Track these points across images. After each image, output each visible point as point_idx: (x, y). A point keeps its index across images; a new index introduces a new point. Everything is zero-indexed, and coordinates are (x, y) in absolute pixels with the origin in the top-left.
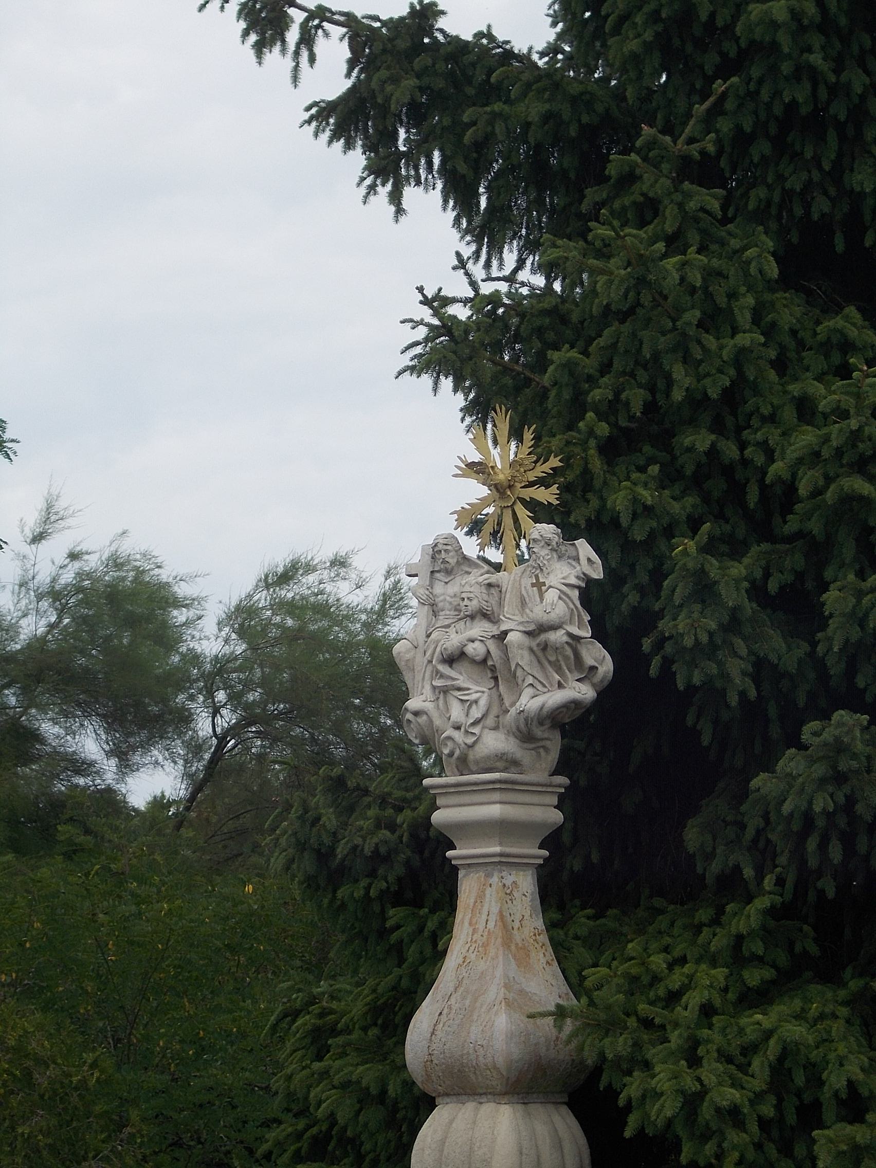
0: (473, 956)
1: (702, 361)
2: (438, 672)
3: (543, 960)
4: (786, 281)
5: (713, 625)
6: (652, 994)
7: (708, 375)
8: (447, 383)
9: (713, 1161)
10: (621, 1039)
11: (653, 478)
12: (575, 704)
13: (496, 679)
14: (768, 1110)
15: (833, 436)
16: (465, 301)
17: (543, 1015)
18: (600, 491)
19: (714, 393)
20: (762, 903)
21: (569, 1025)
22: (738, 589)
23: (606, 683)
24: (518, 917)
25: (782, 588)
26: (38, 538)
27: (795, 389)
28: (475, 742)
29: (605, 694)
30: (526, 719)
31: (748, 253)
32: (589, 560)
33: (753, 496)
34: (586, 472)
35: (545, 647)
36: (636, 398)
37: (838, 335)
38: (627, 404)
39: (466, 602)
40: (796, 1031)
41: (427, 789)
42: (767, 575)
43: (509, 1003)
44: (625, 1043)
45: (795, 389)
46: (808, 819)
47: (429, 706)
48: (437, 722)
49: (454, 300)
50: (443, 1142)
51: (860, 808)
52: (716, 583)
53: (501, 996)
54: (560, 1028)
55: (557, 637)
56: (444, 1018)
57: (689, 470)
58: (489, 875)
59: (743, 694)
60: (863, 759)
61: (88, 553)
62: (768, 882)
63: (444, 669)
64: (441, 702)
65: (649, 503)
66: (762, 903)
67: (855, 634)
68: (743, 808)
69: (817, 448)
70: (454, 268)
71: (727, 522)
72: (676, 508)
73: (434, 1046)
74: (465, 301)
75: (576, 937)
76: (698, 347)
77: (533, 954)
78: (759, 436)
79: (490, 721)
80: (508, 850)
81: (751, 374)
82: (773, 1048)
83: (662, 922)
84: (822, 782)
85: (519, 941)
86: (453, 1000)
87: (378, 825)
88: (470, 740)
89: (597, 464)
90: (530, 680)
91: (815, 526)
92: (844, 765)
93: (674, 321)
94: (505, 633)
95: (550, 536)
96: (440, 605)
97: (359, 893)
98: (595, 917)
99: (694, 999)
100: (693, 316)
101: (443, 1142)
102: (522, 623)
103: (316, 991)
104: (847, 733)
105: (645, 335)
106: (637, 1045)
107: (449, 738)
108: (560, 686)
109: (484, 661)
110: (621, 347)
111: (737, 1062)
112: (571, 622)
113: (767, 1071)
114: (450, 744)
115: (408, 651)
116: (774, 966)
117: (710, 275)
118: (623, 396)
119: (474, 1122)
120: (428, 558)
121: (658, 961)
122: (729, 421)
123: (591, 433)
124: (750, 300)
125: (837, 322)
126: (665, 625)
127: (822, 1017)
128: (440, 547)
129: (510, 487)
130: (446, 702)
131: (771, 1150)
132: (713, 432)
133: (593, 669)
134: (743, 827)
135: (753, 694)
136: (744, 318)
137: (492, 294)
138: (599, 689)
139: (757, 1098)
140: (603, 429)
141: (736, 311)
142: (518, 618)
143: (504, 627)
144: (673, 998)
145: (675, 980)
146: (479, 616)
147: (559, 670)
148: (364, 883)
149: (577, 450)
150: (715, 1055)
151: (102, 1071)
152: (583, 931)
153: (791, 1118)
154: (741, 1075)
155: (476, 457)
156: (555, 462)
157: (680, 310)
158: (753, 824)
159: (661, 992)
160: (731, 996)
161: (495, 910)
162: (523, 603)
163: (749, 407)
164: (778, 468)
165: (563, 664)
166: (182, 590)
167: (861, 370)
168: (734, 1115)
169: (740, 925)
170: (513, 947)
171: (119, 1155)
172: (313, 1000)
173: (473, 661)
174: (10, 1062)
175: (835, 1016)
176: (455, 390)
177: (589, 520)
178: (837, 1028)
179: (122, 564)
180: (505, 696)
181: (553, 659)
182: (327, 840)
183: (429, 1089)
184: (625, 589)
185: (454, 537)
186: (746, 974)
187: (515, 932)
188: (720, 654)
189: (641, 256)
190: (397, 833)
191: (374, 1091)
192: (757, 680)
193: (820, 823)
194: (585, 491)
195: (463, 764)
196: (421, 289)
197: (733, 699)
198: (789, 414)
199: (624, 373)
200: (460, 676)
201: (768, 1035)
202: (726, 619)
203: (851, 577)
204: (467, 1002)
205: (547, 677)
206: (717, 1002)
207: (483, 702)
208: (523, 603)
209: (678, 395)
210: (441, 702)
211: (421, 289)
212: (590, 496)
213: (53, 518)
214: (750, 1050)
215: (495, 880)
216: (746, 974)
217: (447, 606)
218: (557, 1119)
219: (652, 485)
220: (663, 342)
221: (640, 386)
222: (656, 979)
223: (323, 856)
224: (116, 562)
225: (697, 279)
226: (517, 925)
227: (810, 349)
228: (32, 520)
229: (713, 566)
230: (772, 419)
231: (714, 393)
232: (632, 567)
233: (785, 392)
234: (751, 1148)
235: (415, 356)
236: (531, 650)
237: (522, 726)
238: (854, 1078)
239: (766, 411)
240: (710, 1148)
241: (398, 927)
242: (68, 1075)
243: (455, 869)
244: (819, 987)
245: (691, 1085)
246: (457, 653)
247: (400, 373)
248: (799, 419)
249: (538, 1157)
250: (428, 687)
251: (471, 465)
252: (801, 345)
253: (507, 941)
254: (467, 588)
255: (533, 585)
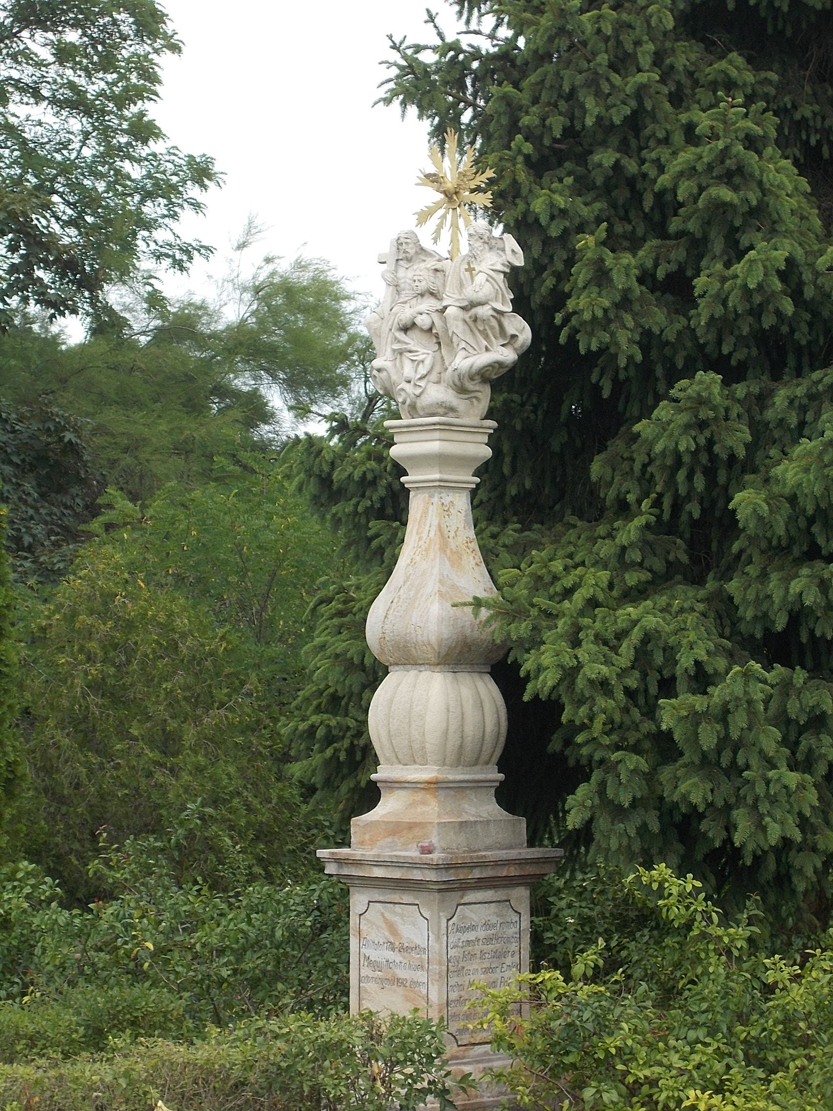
0: (418, 558)
1: (610, 94)
2: (396, 338)
3: (473, 562)
4: (676, 34)
5: (607, 303)
6: (552, 590)
7: (615, 105)
8: (413, 110)
9: (586, 721)
10: (524, 625)
11: (568, 187)
12: (500, 364)
13: (439, 344)
14: (632, 682)
15: (705, 154)
16: (435, 49)
17: (465, 604)
18: (526, 197)
19: (617, 120)
20: (639, 521)
21: (484, 613)
22: (627, 275)
23: (525, 348)
24: (454, 528)
25: (668, 276)
26: (241, 246)
27: (684, 118)
28: (421, 393)
29: (526, 357)
30: (459, 376)
31: (650, 9)
32: (513, 251)
33: (648, 202)
34: (515, 182)
35: (475, 320)
36: (557, 124)
37: (723, 75)
38: (550, 128)
39: (417, 283)
40: (651, 621)
41: (387, 429)
42: (656, 265)
43: (441, 594)
44: (526, 627)
45: (684, 118)
46: (678, 456)
47: (388, 365)
48: (394, 377)
49: (426, 47)
50: (391, 701)
51: (717, 449)
52: (611, 270)
53: (437, 589)
54: (476, 614)
55: (484, 311)
56: (394, 604)
57: (599, 181)
58: (431, 496)
59: (630, 358)
60: (722, 410)
61: (279, 258)
62: (645, 504)
63: (401, 336)
64: (398, 361)
65: (562, 206)
66: (639, 521)
67: (719, 311)
68: (634, 447)
69: (693, 164)
70: (426, 22)
71: (630, 223)
72: (585, 211)
73: (386, 627)
74: (435, 49)
75: (505, 546)
76: (606, 84)
77: (465, 557)
78: (653, 155)
79: (433, 377)
80: (446, 477)
81: (648, 105)
82: (636, 635)
83: (572, 535)
84: (687, 427)
85: (453, 546)
86: (402, 591)
87: (369, 456)
88: (418, 391)
89: (522, 176)
90: (463, 345)
91: (692, 226)
92: (706, 413)
93: (589, 61)
94: (445, 308)
95: (482, 231)
96: (402, 286)
97: (349, 509)
98: (521, 531)
99: (579, 597)
100: (603, 58)
101: (391, 701)
102: (458, 300)
103: (346, 584)
104: (706, 389)
105: (566, 73)
106: (535, 628)
107: (402, 390)
108: (487, 349)
109: (430, 330)
110: (547, 84)
111: (611, 644)
112: (496, 300)
113: (632, 652)
114: (403, 393)
115: (376, 321)
116: (650, 570)
117: (621, 27)
118: (547, 122)
119: (414, 686)
120: (395, 249)
121: (557, 566)
122: (633, 143)
123: (519, 151)
124: (650, 47)
125: (722, 65)
126: (571, 305)
127: (682, 610)
128: (402, 240)
129: (456, 193)
130: (401, 362)
131: (636, 713)
132: (619, 151)
133: (514, 337)
134: (632, 460)
135: (639, 358)
136: (645, 61)
137: (453, 43)
138: (520, 352)
139: (623, 673)
140: (528, 148)
141: (639, 55)
142: (457, 296)
143: (444, 304)
144: (568, 593)
145: (568, 581)
146: (427, 295)
147: (486, 337)
148: (353, 502)
149: (508, 165)
150: (592, 638)
151: (228, 643)
152: (508, 541)
153: (653, 690)
154: (613, 655)
155: (432, 170)
156: (490, 173)
157: (594, 54)
158: (640, 458)
159: (558, 589)
160: (615, 593)
161: (435, 523)
162: (462, 285)
163: (647, 132)
164: (664, 180)
165: (489, 332)
166: (348, 287)
167: (727, 102)
168: (604, 686)
169: (622, 538)
170: (448, 552)
171: (240, 706)
172: (342, 590)
173: (422, 330)
174: (159, 635)
175: (692, 609)
176: (420, 117)
177: (516, 220)
178: (691, 619)
179: (305, 267)
180: (445, 357)
181: (481, 328)
182: (326, 468)
183: (382, 659)
184: (544, 275)
185: (413, 233)
186: (627, 576)
187: (451, 540)
188: (613, 326)
189: (562, 10)
190: (383, 465)
191: (356, 661)
192: (645, 348)
193: (686, 459)
194: (514, 197)
195: (413, 409)
196: (390, 37)
197: (622, 362)
198: (678, 138)
199: (549, 104)
200: (412, 341)
201: (635, 623)
202: (618, 299)
203: (719, 266)
204: (412, 593)
205: (477, 343)
206: (601, 597)
207: (428, 362)
208: (462, 285)
209: (589, 121)
210: (398, 361)
211: (390, 37)
212: (518, 201)
213: (253, 231)
214: (621, 635)
215: (436, 500)
216: (627, 576)
217: (407, 287)
218: (480, 684)
219: (567, 193)
220: (579, 79)
221: (560, 114)
222: (555, 578)
223: (325, 481)
224: (300, 266)
225: (608, 30)
226: (452, 534)
227: (702, 86)
228: (238, 236)
229: (609, 258)
230: (666, 141)
231: (617, 120)
232: (551, 257)
233: (678, 120)
234: (618, 712)
235: (390, 90)
236: (465, 321)
237: (457, 381)
238: (700, 659)
239: (661, 135)
240: (583, 711)
241: (377, 535)
242: (203, 645)
243: (408, 491)
244: (684, 587)
245: (570, 662)
246: (409, 323)
247: (376, 103)
248: (687, 142)
249: (463, 714)
250: (389, 351)
251: (428, 176)
252: (696, 83)
253: (444, 546)
254: (418, 273)
255: (466, 270)
